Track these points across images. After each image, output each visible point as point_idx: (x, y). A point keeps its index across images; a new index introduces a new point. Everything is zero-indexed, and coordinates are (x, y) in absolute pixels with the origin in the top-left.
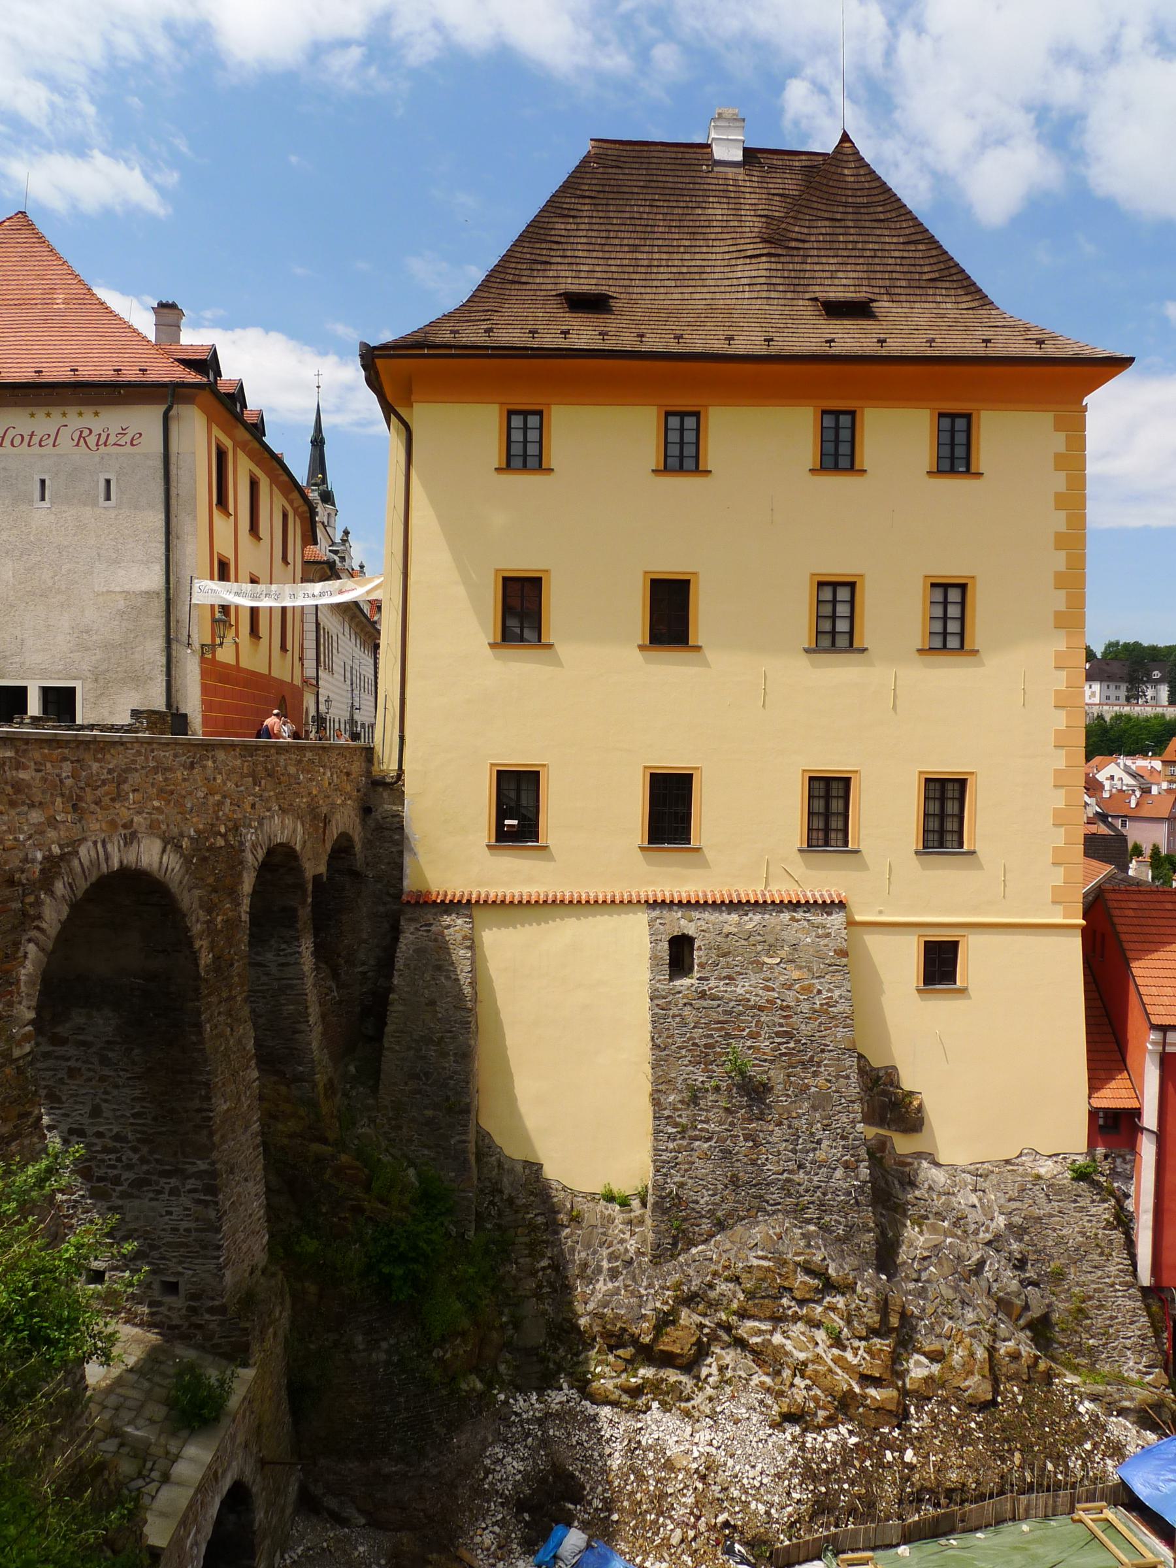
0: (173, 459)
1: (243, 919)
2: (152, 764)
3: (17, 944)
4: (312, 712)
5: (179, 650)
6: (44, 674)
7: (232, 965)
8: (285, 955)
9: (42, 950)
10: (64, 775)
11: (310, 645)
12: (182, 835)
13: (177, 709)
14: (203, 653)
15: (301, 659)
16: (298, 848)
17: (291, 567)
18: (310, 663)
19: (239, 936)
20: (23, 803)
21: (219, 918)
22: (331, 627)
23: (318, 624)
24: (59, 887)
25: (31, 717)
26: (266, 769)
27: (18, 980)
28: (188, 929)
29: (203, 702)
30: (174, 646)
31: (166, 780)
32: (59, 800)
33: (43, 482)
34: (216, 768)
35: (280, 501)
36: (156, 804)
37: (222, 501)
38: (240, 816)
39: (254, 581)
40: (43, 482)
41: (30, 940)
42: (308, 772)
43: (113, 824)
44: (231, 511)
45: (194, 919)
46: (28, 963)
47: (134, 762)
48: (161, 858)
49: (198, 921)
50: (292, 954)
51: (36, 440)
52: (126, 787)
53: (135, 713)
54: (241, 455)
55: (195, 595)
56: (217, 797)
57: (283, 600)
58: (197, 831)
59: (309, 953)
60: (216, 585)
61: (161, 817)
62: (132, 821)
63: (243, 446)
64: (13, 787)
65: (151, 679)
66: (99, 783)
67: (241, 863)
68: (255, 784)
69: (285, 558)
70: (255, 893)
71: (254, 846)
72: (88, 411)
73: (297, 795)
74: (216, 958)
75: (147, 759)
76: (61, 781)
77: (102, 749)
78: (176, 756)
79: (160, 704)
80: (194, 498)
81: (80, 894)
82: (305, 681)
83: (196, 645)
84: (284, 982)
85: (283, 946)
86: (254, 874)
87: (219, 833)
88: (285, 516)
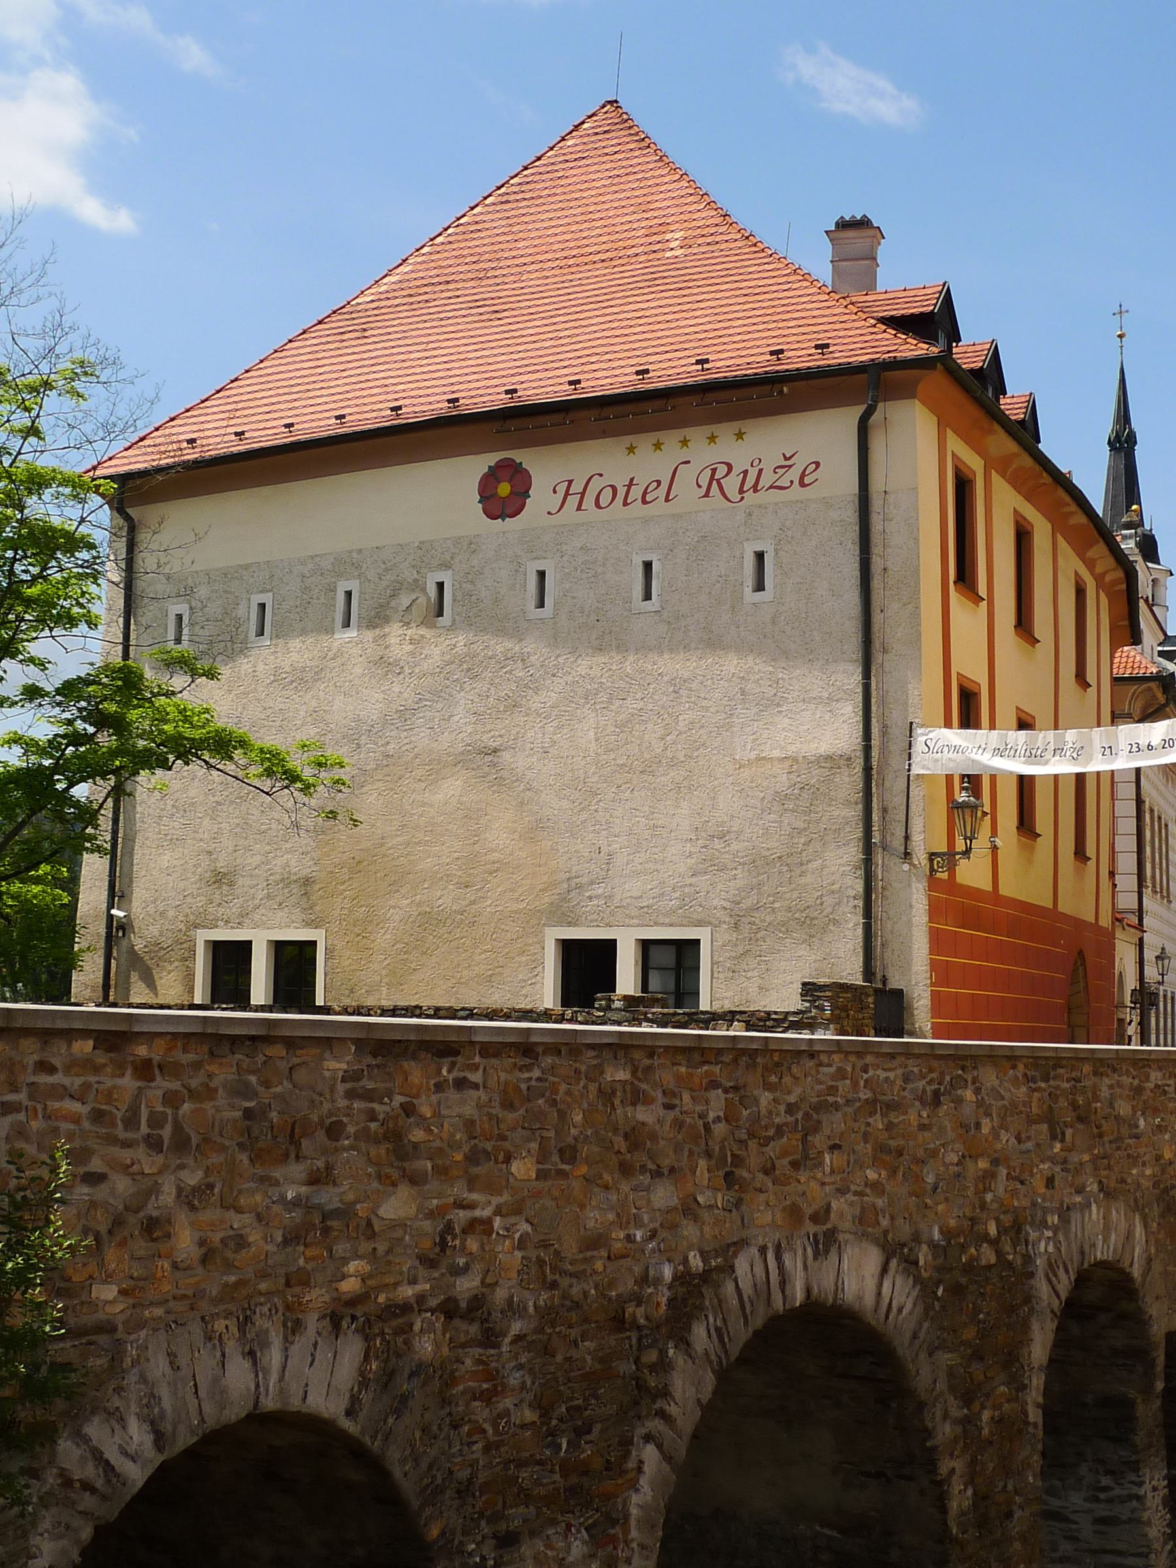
0: (876, 504)
1: (1031, 1419)
2: (865, 1095)
3: (626, 1443)
4: (1131, 983)
5: (888, 867)
6: (646, 916)
7: (1009, 1515)
8: (1110, 1501)
9: (668, 1458)
10: (712, 1115)
11: (1126, 843)
12: (916, 1238)
13: (884, 980)
14: (932, 870)
15: (1112, 874)
16: (1136, 1272)
17: (1092, 691)
18: (1127, 882)
19: (1025, 1453)
20: (643, 1168)
21: (986, 1415)
22: (1162, 802)
23: (1139, 802)
24: (699, 1334)
25: (625, 998)
26: (1074, 1106)
27: (627, 1517)
28: (928, 1433)
29: (934, 966)
30: (878, 858)
31: (890, 1127)
32: (702, 1164)
33: (648, 566)
34: (980, 1104)
35: (1071, 563)
36: (871, 1175)
37: (965, 575)
38: (1025, 1203)
39: (1024, 724)
40: (648, 566)
41: (648, 1438)
42: (1156, 1111)
43: (794, 1213)
44: (982, 591)
45: (939, 1414)
46: (644, 1482)
47: (833, 1090)
48: (880, 1285)
49: (946, 1416)
50: (1123, 1500)
51: (636, 492)
52: (818, 1140)
53: (809, 989)
54: (999, 484)
55: (916, 759)
56: (983, 1164)
57: (1090, 759)
58: (946, 1233)
59: (1158, 1500)
60: (956, 736)
61: (880, 1202)
62: (828, 1209)
63: (998, 464)
64: (626, 1136)
65: (836, 922)
66: (771, 1132)
67: (1027, 1300)
68: (1053, 1137)
69: (1081, 676)
70: (1056, 1364)
71: (1051, 1266)
72: (725, 431)
73: (1134, 1159)
74: (981, 1498)
75: (855, 1084)
76: (707, 1127)
77: (777, 1065)
78: (907, 1079)
79: (851, 972)
80: (916, 572)
81: (735, 1351)
82: (1117, 920)
83: (920, 856)
84: (1109, 1559)
85: (1105, 1481)
86: (1051, 1325)
87: (986, 1238)
88: (1080, 592)
